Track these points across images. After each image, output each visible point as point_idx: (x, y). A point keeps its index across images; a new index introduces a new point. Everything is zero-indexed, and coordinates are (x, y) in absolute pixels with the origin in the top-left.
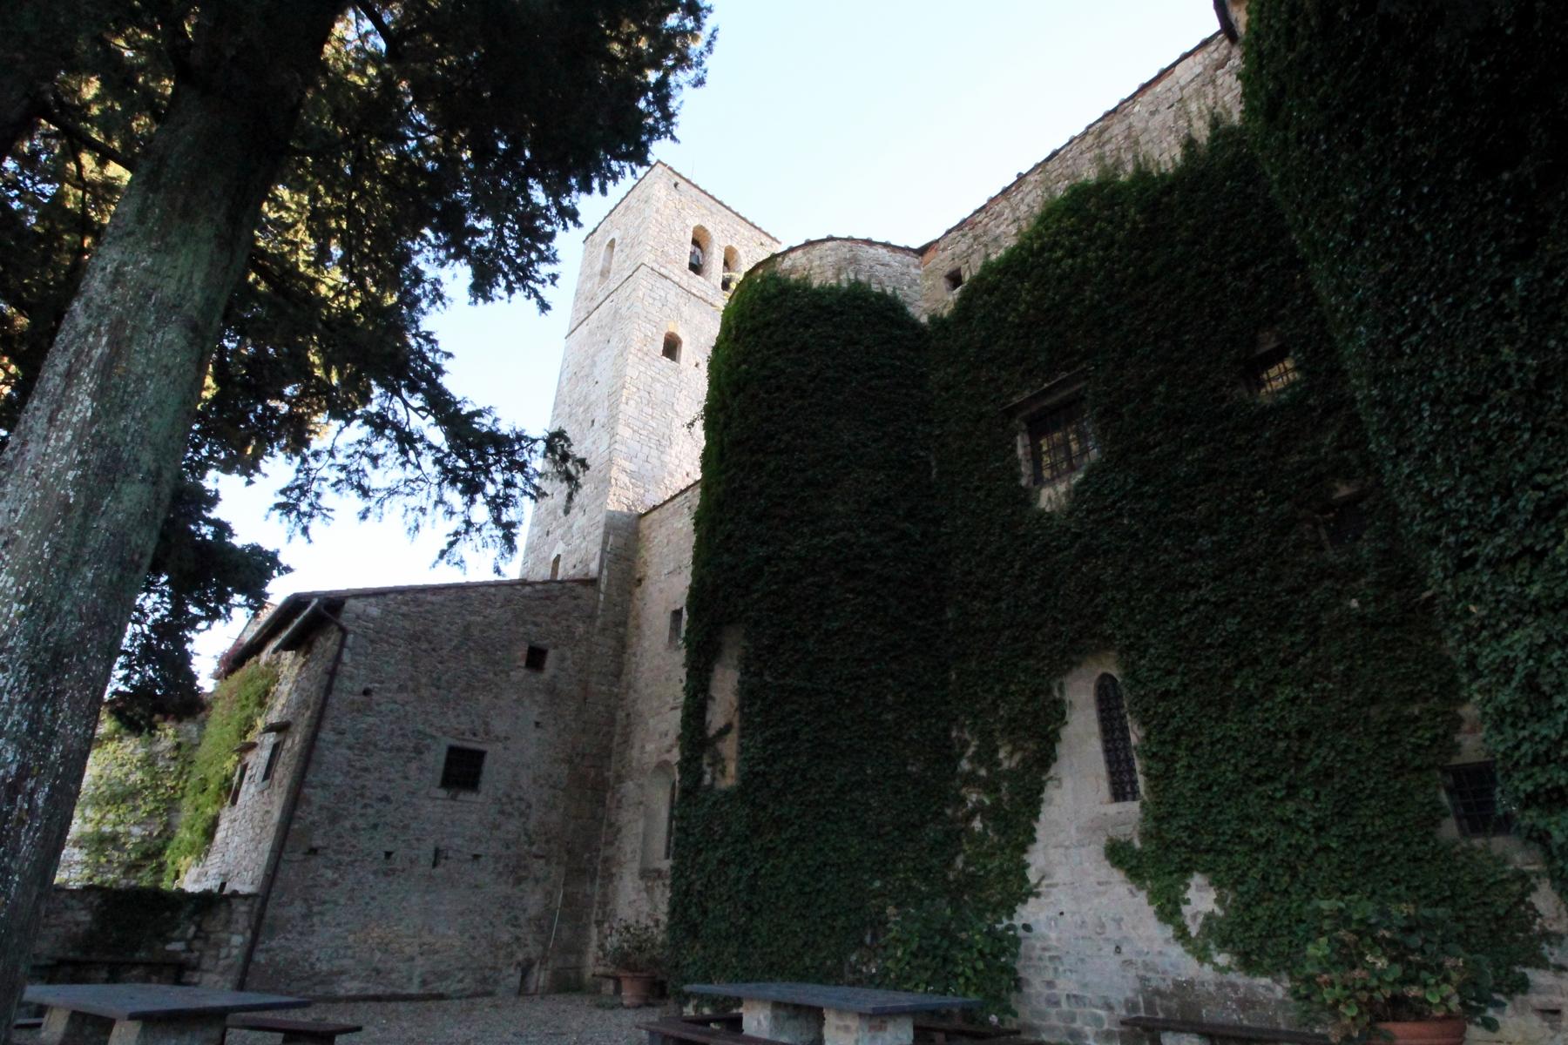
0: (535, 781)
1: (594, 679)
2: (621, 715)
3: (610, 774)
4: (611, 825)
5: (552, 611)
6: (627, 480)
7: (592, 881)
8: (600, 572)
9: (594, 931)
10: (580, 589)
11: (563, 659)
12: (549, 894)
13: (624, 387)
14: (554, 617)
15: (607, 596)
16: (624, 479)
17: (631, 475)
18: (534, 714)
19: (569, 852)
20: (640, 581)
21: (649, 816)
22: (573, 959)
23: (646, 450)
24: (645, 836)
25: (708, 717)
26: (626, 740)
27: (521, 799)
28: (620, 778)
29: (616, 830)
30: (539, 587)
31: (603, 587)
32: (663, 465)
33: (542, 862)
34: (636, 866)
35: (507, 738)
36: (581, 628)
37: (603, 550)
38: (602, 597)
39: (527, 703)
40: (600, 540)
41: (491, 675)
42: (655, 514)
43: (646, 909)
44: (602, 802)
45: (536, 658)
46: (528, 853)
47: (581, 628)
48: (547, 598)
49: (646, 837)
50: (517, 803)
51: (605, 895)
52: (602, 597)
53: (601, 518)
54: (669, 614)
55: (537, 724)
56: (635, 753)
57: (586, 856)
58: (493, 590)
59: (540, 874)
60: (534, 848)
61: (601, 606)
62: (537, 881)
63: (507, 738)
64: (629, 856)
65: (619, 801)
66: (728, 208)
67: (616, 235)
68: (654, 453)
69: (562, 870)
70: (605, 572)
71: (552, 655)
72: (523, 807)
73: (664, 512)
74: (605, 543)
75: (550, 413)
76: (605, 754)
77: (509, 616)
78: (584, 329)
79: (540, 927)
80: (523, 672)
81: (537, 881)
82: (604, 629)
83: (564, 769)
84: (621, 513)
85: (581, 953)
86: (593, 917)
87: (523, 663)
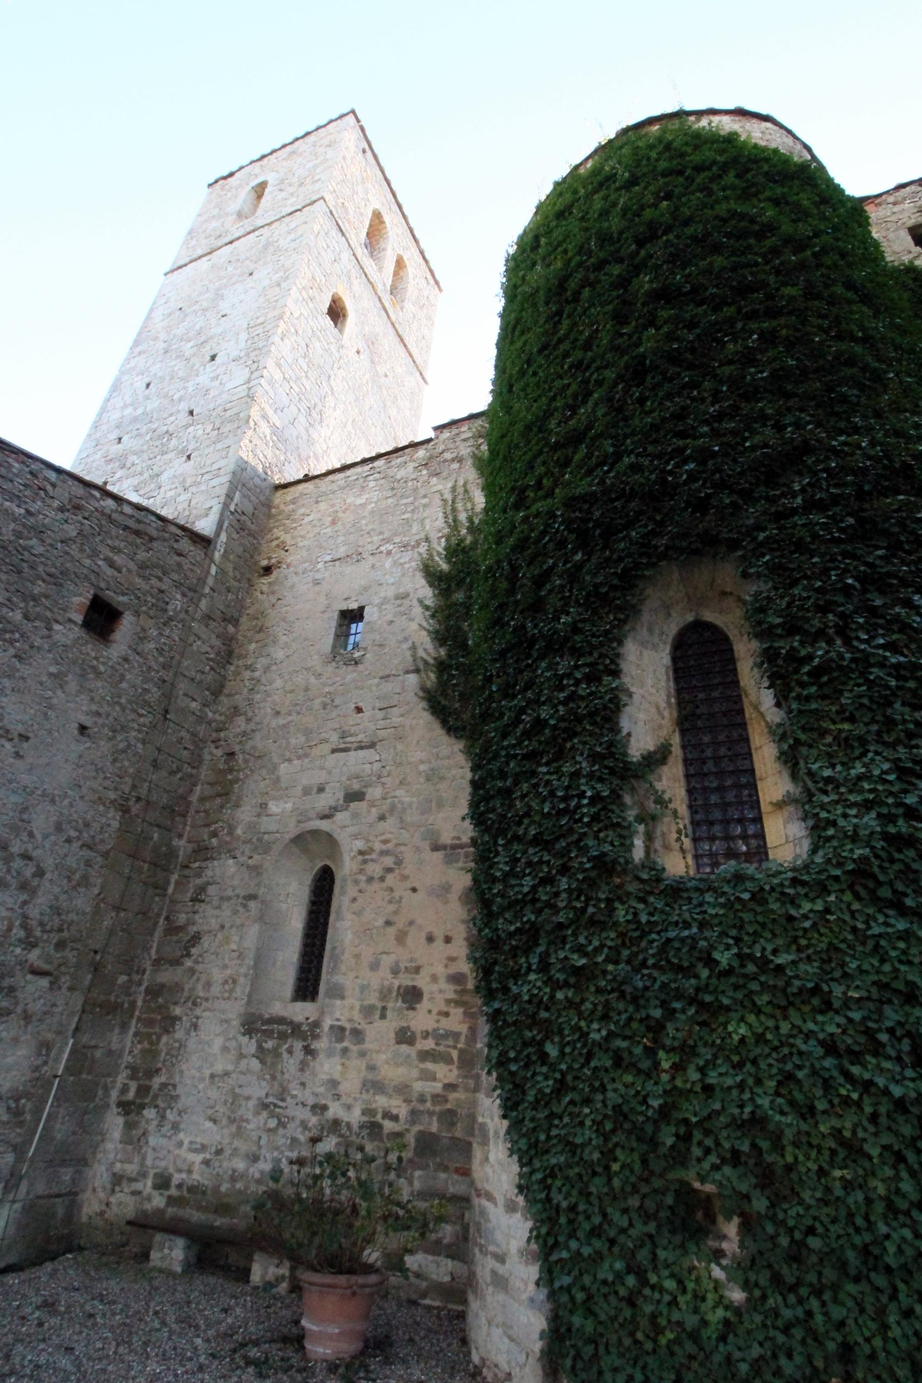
0: (59, 828)
1: (182, 686)
2: (213, 754)
3: (182, 845)
4: (173, 929)
5: (142, 555)
6: (268, 432)
7: (124, 1026)
8: (218, 534)
9: (114, 1123)
10: (185, 545)
11: (142, 637)
12: (45, 1047)
13: (281, 317)
14: (142, 566)
15: (221, 571)
16: (265, 429)
17: (275, 430)
18: (79, 710)
19: (96, 968)
20: (268, 570)
21: (268, 920)
22: (67, 1175)
23: (293, 409)
24: (259, 959)
25: (625, 724)
26: (225, 789)
27: (26, 857)
28: (202, 852)
29: (185, 942)
30: (127, 509)
31: (217, 556)
32: (310, 442)
33: (44, 982)
34: (234, 1010)
35: (24, 738)
36: (177, 602)
37: (226, 506)
38: (213, 570)
39: (72, 685)
40: (222, 491)
41: (17, 616)
42: (309, 486)
43: (258, 1090)
44: (160, 888)
45: (101, 618)
46: (22, 963)
47: (177, 602)
48: (137, 533)
49: (261, 962)
50: (18, 863)
51: (151, 1053)
52: (213, 570)
53: (228, 465)
54: (336, 615)
55: (83, 729)
56: (245, 814)
57: (122, 979)
58: (53, 476)
59: (37, 1007)
60: (34, 956)
61: (210, 581)
62: (27, 1017)
63: (24, 738)
64: (215, 990)
65: (202, 889)
66: (405, 217)
67: (271, 178)
68: (302, 419)
69: (78, 1000)
70: (223, 537)
71: (126, 626)
72: (29, 871)
73: (324, 484)
74: (229, 497)
75: (127, 349)
76: (177, 809)
77: (71, 531)
78: (204, 264)
79: (17, 1113)
80: (77, 632)
81: (27, 1017)
82: (208, 617)
83: (114, 820)
84: (254, 469)
85: (82, 1162)
86: (114, 1094)
87: (79, 618)
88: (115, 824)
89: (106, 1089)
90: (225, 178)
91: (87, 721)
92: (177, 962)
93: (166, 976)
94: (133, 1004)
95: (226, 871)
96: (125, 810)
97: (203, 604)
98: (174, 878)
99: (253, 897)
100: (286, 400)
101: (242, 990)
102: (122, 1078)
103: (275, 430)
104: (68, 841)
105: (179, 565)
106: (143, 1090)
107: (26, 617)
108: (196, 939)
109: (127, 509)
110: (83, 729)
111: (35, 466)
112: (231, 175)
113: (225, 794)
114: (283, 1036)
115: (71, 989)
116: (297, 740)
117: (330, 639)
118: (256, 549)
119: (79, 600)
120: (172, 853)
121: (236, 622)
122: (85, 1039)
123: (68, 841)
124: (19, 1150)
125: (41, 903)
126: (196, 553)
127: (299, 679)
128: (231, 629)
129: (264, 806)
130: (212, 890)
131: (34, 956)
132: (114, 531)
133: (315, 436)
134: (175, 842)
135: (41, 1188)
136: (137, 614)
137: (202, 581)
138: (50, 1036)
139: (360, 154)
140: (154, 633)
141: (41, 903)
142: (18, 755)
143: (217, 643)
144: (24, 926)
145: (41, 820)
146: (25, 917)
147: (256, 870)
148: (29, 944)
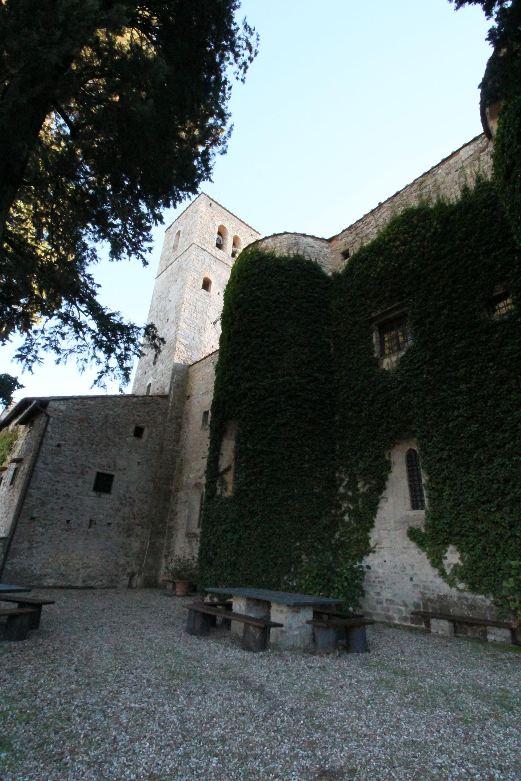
0: (137, 490)
2: (178, 460)
3: (173, 488)
5: (147, 410)
6: (184, 348)
7: (163, 537)
8: (170, 392)
9: (163, 561)
10: (160, 400)
11: (151, 433)
12: (143, 543)
16: (182, 348)
17: (185, 346)
23: (193, 334)
26: (181, 472)
27: (130, 498)
28: (177, 490)
30: (140, 398)
31: (171, 399)
33: (140, 527)
35: (124, 469)
37: (172, 382)
38: (170, 404)
40: (170, 377)
42: (197, 365)
45: (138, 432)
48: (144, 404)
53: (171, 366)
55: (139, 463)
56: (185, 478)
57: (161, 525)
58: (119, 399)
59: (140, 533)
60: (137, 521)
61: (170, 408)
63: (124, 469)
65: (177, 500)
67: (181, 228)
68: (197, 336)
70: (172, 392)
71: (146, 432)
74: (172, 378)
76: (170, 478)
77: (126, 411)
78: (164, 274)
80: (132, 438)
82: (171, 420)
83: (152, 485)
84: (180, 364)
85: (157, 570)
87: (132, 434)
88: (152, 486)
89: (161, 553)
90: (169, 228)
91: (140, 461)
92: (173, 520)
93: (171, 524)
94: (165, 532)
95: (181, 494)
96: (154, 482)
97: (169, 416)
98: (172, 497)
99: (186, 502)
100: (189, 332)
101: (185, 526)
102: (165, 550)
103: (185, 346)
104: (140, 492)
105: (159, 408)
106: (168, 552)
107: (119, 439)
108: (176, 514)
109: (140, 398)
110: (139, 463)
111: (113, 399)
112: (171, 226)
113: (180, 473)
114: (192, 537)
115: (147, 528)
116: (195, 455)
117: (201, 422)
118: (185, 391)
119: (131, 429)
120: (170, 491)
121: (181, 417)
122: (153, 541)
123: (140, 492)
124: (140, 565)
125: (136, 510)
126: (164, 401)
127: (195, 435)
128: (179, 420)
129: (188, 475)
130: (179, 500)
131: (137, 521)
132: (138, 406)
133: (203, 339)
134: (171, 487)
135: (147, 574)
136: (148, 427)
137: (167, 409)
138: (144, 540)
139: (209, 208)
140: (154, 430)
141: (136, 510)
142: (124, 474)
143: (175, 426)
144: (133, 514)
145: (132, 489)
146: (133, 513)
147: (187, 494)
148: (135, 518)
